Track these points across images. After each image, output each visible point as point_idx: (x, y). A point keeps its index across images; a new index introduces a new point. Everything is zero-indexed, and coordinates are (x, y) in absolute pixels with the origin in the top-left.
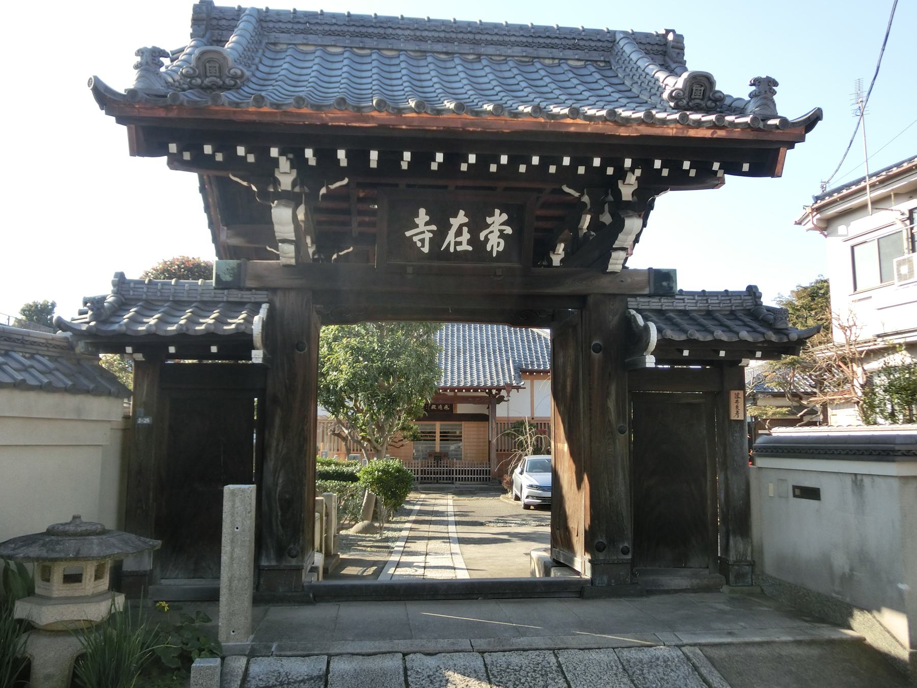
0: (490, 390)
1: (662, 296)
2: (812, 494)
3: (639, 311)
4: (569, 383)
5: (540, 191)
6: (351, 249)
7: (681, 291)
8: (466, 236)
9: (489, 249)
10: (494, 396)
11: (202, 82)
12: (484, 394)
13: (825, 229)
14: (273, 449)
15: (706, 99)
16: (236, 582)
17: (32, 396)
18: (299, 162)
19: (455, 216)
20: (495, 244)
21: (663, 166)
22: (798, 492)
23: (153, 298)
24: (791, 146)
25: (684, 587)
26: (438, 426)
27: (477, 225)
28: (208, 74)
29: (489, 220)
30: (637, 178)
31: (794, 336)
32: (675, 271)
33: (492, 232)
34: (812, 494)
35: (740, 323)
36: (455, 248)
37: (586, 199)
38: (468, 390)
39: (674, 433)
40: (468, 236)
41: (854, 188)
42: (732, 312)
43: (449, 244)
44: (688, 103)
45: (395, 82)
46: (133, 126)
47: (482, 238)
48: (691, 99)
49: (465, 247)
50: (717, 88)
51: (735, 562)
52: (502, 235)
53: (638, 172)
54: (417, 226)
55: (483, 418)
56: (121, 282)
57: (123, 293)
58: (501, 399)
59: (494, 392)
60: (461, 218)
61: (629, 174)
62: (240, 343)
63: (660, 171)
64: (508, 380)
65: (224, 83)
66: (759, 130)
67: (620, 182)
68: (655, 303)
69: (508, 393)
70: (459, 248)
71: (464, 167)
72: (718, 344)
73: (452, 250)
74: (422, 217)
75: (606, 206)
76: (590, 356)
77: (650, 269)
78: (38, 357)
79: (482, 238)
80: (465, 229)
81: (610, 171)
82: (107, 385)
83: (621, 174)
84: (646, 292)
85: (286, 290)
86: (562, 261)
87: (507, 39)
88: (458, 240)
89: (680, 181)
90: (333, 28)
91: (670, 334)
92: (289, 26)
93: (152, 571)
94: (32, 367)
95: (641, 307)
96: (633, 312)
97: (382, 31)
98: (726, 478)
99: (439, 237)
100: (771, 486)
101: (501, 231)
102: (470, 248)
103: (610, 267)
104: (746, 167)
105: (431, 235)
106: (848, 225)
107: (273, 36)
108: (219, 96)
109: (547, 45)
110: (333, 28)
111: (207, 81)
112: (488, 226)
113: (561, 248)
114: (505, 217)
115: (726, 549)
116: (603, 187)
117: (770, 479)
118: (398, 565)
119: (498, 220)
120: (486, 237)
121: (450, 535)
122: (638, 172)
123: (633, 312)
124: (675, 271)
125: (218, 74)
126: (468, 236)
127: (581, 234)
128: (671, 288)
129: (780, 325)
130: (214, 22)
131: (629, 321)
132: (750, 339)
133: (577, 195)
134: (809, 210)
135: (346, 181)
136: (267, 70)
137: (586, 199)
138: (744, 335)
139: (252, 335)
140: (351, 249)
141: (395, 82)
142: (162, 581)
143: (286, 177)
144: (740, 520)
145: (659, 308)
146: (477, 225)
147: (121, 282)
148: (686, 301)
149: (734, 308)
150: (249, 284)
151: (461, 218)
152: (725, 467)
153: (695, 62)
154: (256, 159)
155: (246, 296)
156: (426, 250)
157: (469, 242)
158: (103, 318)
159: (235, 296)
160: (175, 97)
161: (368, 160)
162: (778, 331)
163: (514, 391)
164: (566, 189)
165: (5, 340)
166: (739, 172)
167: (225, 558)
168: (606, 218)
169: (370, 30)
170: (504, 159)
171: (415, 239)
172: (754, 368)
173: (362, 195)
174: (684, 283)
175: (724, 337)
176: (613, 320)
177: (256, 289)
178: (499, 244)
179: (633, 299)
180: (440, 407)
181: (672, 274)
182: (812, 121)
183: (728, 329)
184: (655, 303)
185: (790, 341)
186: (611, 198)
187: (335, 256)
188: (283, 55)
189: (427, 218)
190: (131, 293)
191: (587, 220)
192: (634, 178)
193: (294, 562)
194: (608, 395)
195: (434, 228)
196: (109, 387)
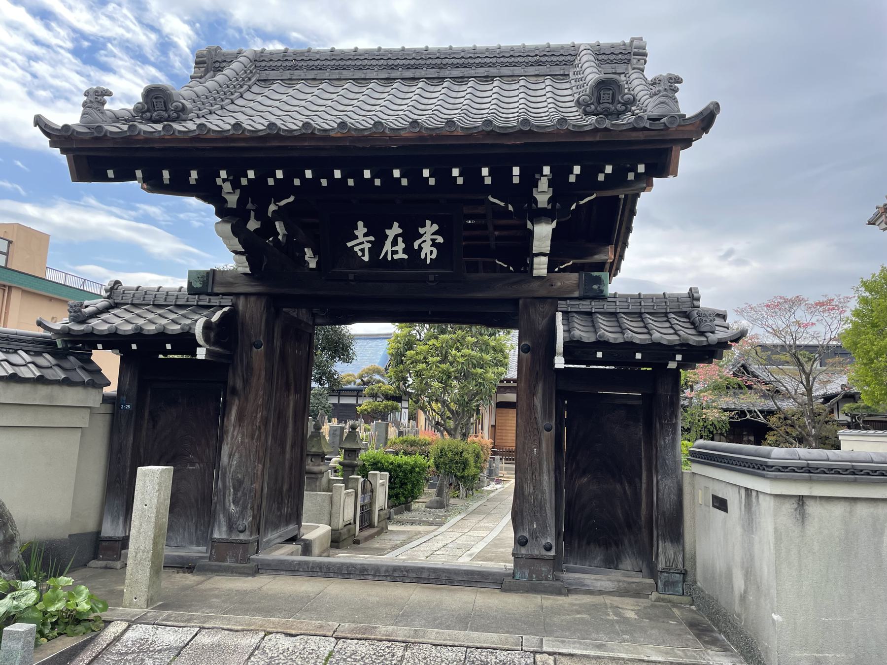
8: (401, 246)
9: (423, 257)
14: (230, 434)
20: (428, 253)
21: (402, 176)
25: (611, 590)
27: (410, 235)
29: (421, 231)
32: (190, 272)
33: (425, 241)
37: (510, 208)
40: (403, 246)
44: (596, 108)
45: (539, 99)
47: (416, 247)
49: (401, 255)
52: (434, 244)
54: (357, 237)
60: (396, 230)
62: (186, 341)
70: (396, 257)
71: (601, 177)
73: (389, 258)
74: (361, 229)
79: (416, 247)
80: (400, 239)
84: (576, 294)
85: (247, 295)
87: (472, 61)
88: (394, 249)
90: (316, 63)
92: (279, 63)
97: (358, 63)
99: (377, 247)
102: (406, 257)
103: (535, 271)
109: (510, 63)
110: (316, 63)
112: (421, 236)
114: (436, 227)
119: (429, 230)
120: (420, 246)
124: (190, 272)
126: (403, 246)
128: (602, 291)
130: (217, 65)
141: (539, 99)
143: (543, 195)
144: (674, 526)
145: (589, 310)
146: (410, 235)
150: (217, 290)
151: (396, 230)
156: (366, 258)
157: (405, 251)
159: (205, 300)
169: (348, 63)
170: (279, 174)
171: (356, 249)
178: (432, 252)
179: (564, 302)
182: (706, 120)
189: (365, 230)
195: (372, 238)
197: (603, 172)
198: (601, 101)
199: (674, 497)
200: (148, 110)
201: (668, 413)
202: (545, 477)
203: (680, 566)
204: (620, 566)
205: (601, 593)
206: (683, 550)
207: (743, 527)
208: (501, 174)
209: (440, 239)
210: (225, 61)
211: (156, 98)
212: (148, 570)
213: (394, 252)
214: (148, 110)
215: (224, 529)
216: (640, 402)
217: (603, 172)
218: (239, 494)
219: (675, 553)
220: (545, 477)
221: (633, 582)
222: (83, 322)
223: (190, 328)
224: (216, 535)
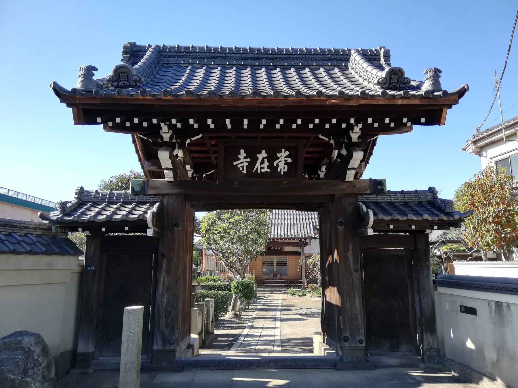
0: (301, 240)
1: (378, 194)
2: (472, 311)
3: (364, 203)
4: (328, 242)
5: (308, 138)
6: (213, 171)
7: (389, 191)
8: (266, 164)
9: (279, 170)
10: (303, 243)
11: (118, 84)
12: (298, 241)
13: (480, 152)
15: (399, 83)
16: (129, 364)
17: (21, 257)
18: (171, 127)
19: (260, 153)
20: (282, 168)
21: (390, 121)
22: (463, 309)
23: (97, 200)
24: (450, 107)
26: (275, 258)
27: (272, 157)
28: (121, 80)
29: (279, 155)
30: (360, 129)
31: (457, 217)
32: (385, 180)
33: (281, 161)
34: (472, 311)
35: (425, 209)
36: (261, 171)
37: (332, 141)
38: (289, 239)
39: (389, 273)
40: (268, 164)
41: (495, 130)
42: (420, 203)
43: (257, 168)
44: (388, 86)
46: (76, 109)
47: (275, 165)
48: (390, 83)
49: (266, 170)
50: (406, 76)
51: (427, 349)
52: (286, 163)
53: (360, 126)
54: (240, 159)
55: (298, 254)
56: (81, 192)
57: (82, 198)
58: (307, 244)
59: (303, 240)
60: (264, 154)
61: (355, 127)
62: (140, 224)
63: (389, 124)
64: (310, 234)
65: (130, 84)
66: (430, 98)
67: (350, 132)
68: (374, 198)
69: (310, 241)
70: (263, 171)
71: (294, 126)
72: (413, 222)
73: (259, 172)
74: (242, 154)
75: (344, 145)
76: (337, 228)
77: (370, 179)
78: (29, 235)
79: (275, 165)
80: (266, 160)
81: (344, 126)
82: (72, 249)
83: (351, 127)
84: (369, 192)
85: (169, 195)
86: (325, 175)
87: (291, 56)
88: (262, 166)
89: (386, 130)
91: (381, 216)
93: (93, 352)
94: (23, 241)
95: (365, 201)
96: (361, 204)
98: (420, 298)
100: (447, 304)
101: (285, 161)
102: (269, 170)
104: (423, 120)
105: (247, 164)
106: (486, 152)
107: (166, 60)
108: (121, 91)
111: (120, 84)
112: (278, 158)
113: (324, 168)
114: (287, 153)
115: (422, 341)
116: (341, 135)
117: (447, 299)
118: (247, 336)
119: (283, 154)
121: (277, 316)
122: (360, 126)
123: (361, 204)
124: (385, 180)
125: (126, 79)
126: (268, 164)
127: (333, 161)
128: (383, 190)
129: (448, 210)
130: (135, 53)
131: (358, 209)
132: (430, 218)
133: (327, 139)
134: (470, 142)
135: (200, 136)
136: (160, 77)
137: (332, 141)
138: (426, 217)
139: (147, 221)
140: (213, 171)
142: (100, 358)
143: (166, 135)
144: (430, 324)
145: (376, 201)
146: (272, 157)
147: (81, 192)
148: (392, 197)
149: (421, 200)
150: (150, 192)
151: (264, 154)
152: (419, 293)
153: (395, 63)
154: (198, 126)
155: (148, 199)
156: (245, 172)
157: (268, 167)
158: (66, 213)
159: (143, 198)
160: (97, 92)
161: (242, 124)
162: (447, 214)
163: (313, 240)
164: (321, 136)
165: (9, 227)
166: (419, 123)
167: (123, 350)
168: (344, 152)
171: (239, 166)
172: (435, 235)
173: (213, 143)
174: (390, 187)
175: (414, 218)
176: (350, 209)
177: (154, 195)
178: (284, 168)
179: (361, 196)
180: (276, 248)
181: (383, 182)
182: (461, 93)
183: (417, 213)
184: (374, 198)
185: (454, 220)
186: (346, 140)
187: (204, 175)
188: (170, 70)
189: (245, 155)
190: (86, 198)
191: (336, 153)
192: (358, 129)
193: (172, 347)
194: (348, 251)
195: (249, 160)
196: (69, 250)
197: (279, 123)
198: (392, 82)
199: (430, 307)
200: (116, 81)
201: (424, 259)
202: (357, 299)
203: (436, 347)
204: (400, 350)
205: (392, 366)
206: (437, 338)
207: (494, 323)
208: (237, 124)
209: (290, 160)
210: (141, 51)
211: (122, 73)
212: (135, 375)
213: (262, 168)
214: (116, 81)
215: (160, 343)
216: (404, 253)
217: (279, 123)
218: (169, 320)
219: (433, 340)
220: (357, 299)
221: (409, 359)
222: (69, 215)
223: (144, 216)
224: (155, 347)
